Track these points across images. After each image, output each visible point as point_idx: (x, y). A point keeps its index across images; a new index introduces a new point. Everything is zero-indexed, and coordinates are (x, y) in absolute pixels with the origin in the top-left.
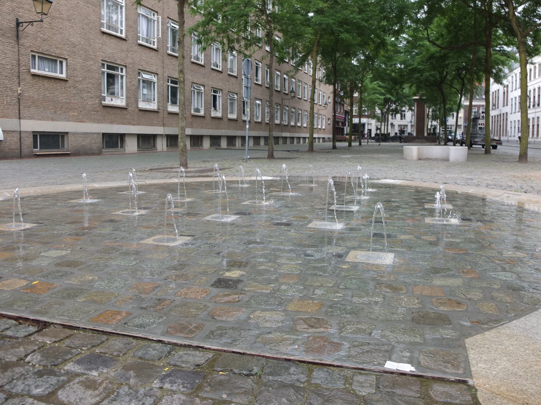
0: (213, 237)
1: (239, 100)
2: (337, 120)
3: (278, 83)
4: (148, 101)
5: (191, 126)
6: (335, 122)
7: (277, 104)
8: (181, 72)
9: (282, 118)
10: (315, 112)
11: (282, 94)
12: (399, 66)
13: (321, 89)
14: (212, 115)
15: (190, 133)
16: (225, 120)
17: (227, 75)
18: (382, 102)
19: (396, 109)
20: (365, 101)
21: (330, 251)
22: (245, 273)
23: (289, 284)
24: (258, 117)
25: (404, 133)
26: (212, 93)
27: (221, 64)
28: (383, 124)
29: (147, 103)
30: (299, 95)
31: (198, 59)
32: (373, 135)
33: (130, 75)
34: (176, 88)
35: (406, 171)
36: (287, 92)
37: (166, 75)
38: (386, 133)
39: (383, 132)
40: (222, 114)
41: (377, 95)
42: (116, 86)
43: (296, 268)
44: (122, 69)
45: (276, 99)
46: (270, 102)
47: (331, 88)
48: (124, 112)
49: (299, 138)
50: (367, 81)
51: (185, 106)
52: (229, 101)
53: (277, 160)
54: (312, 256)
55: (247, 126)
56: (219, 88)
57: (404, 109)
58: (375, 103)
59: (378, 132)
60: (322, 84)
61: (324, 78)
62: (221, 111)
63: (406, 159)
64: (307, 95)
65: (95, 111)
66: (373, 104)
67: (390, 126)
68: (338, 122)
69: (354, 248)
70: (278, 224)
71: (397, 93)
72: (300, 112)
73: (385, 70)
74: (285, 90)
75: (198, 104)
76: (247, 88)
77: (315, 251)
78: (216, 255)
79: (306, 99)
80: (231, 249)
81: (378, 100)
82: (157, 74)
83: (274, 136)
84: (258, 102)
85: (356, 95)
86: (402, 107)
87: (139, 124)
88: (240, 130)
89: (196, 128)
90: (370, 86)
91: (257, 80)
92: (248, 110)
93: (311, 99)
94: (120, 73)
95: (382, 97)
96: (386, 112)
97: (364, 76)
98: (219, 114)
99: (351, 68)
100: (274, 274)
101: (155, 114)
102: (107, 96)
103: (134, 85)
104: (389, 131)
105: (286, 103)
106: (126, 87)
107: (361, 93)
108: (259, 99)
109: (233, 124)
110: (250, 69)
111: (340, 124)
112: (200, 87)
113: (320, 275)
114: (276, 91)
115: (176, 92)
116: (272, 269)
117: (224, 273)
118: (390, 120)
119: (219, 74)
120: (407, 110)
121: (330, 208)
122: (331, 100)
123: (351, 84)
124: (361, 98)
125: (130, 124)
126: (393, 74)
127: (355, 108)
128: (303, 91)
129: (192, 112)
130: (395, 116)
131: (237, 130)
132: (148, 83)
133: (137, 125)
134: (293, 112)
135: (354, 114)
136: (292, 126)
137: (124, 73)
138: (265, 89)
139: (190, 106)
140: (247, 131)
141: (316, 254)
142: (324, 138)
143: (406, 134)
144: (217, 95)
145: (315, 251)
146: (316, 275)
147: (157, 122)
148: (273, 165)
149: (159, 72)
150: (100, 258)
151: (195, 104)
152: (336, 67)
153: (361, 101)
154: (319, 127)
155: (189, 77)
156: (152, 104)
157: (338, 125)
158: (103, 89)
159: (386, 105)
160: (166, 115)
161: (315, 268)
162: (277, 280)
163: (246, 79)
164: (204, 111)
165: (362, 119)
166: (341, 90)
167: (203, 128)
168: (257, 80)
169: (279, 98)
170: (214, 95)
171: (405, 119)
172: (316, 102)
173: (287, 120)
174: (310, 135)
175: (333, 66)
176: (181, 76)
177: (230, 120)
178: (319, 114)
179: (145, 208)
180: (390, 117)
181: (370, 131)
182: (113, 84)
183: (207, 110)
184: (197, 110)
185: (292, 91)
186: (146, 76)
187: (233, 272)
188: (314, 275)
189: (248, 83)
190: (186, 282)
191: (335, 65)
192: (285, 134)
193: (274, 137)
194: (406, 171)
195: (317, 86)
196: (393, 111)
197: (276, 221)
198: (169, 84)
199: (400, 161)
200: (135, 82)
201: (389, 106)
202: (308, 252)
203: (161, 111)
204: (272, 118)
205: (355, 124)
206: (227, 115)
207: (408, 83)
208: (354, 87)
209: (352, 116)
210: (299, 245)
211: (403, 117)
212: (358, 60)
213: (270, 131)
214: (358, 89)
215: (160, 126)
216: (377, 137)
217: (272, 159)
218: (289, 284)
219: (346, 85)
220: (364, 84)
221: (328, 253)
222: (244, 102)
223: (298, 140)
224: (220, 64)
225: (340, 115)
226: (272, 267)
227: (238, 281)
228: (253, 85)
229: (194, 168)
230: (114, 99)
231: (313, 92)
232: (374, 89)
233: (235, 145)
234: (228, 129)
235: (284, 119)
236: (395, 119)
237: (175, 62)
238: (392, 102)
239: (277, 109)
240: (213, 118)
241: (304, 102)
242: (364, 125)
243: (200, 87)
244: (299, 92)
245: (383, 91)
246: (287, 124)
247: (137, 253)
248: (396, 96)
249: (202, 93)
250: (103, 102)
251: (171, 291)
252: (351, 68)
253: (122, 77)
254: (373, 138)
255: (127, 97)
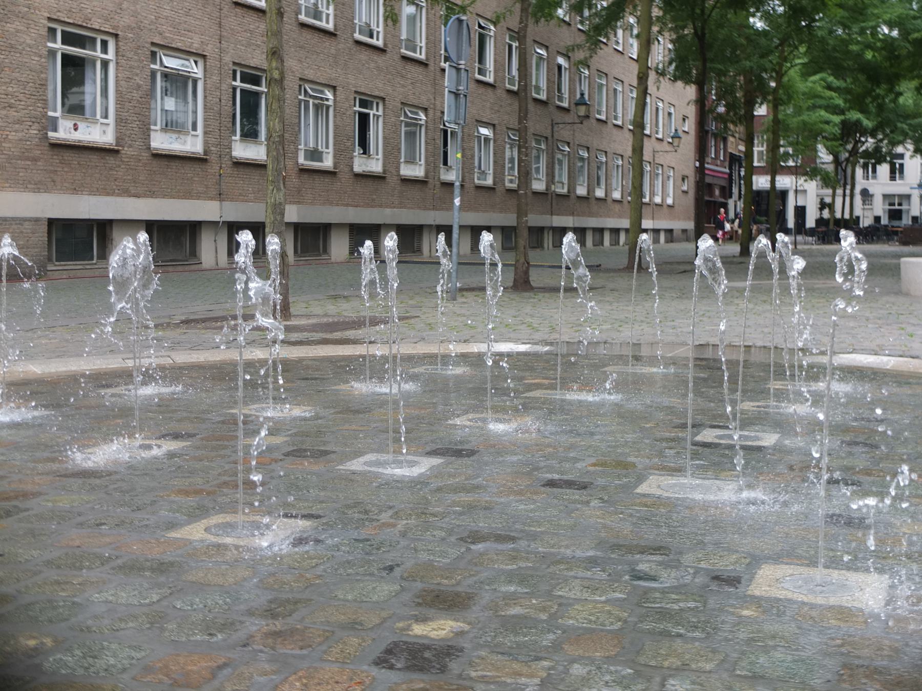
0: (372, 520)
1: (431, 126)
2: (708, 180)
3: (540, 80)
4: (172, 126)
5: (297, 197)
6: (703, 186)
7: (539, 138)
8: (274, 53)
9: (553, 177)
10: (644, 158)
11: (551, 108)
12: (886, 31)
13: (661, 94)
14: (357, 169)
15: (294, 219)
16: (392, 180)
17: (397, 58)
18: (837, 131)
19: (877, 149)
20: (787, 129)
21: (703, 565)
22: (466, 627)
23: (592, 661)
24: (483, 174)
25: (900, 218)
26: (357, 108)
27: (381, 29)
28: (839, 191)
29: (174, 136)
30: (599, 113)
31: (317, 15)
32: (810, 223)
33: (129, 59)
34: (257, 95)
35: (910, 329)
36: (565, 104)
37: (227, 59)
38: (847, 216)
39: (838, 215)
40: (384, 165)
41: (823, 113)
42: (88, 88)
43: (609, 612)
44: (104, 44)
45: (537, 123)
46: (522, 131)
47: (691, 91)
48: (111, 160)
49: (601, 231)
50: (793, 73)
51: (281, 144)
52: (403, 129)
53: (540, 295)
54: (653, 579)
55: (457, 201)
56: (376, 93)
57: (900, 149)
58: (817, 135)
59: (826, 214)
60: (665, 83)
61: (670, 63)
62: (380, 156)
63: (907, 294)
64: (625, 111)
65: (27, 159)
66: (809, 136)
67: (858, 199)
68: (710, 187)
69: (777, 559)
70: (551, 484)
71: (881, 108)
72: (604, 159)
73: (845, 43)
74: (560, 99)
75: (318, 141)
76: (456, 95)
77: (660, 563)
78: (384, 574)
79: (619, 123)
80: (424, 556)
81: (826, 127)
82: (204, 57)
83: (530, 224)
84: (484, 131)
85: (761, 111)
86: (894, 144)
87: (152, 194)
88: (434, 208)
89: (312, 204)
90: (802, 86)
91: (481, 72)
92: (455, 156)
93: (634, 123)
94: (99, 53)
95: (837, 119)
96: (847, 160)
97: (785, 59)
98: (375, 166)
99: (748, 38)
100: (549, 631)
101: (197, 167)
102: (63, 117)
103: (139, 86)
104: (858, 212)
105: (564, 133)
106: (117, 91)
107: (775, 106)
108: (486, 124)
109: (414, 193)
110: (465, 45)
111: (717, 192)
112: (322, 92)
113: (679, 635)
114: (536, 100)
115: (257, 106)
116: (544, 617)
117: (408, 628)
118: (861, 182)
119: (375, 56)
120: (908, 155)
121: (699, 438)
122: (690, 126)
123: (748, 82)
124: (776, 121)
125: (126, 193)
126: (869, 55)
127: (759, 148)
128: (612, 102)
129: (301, 160)
130: (874, 171)
131: (426, 209)
132: (178, 83)
133: (145, 196)
134: (582, 159)
135: (756, 164)
136: (580, 198)
137: (111, 55)
138: (504, 95)
139: (296, 142)
140: (456, 213)
141: (664, 574)
142: (670, 232)
143: (906, 221)
144: (372, 113)
145: (660, 563)
146: (666, 634)
147: (201, 189)
148: (528, 309)
149: (209, 50)
150: (58, 583)
151: (308, 137)
152: (704, 34)
153: (777, 128)
154: (658, 200)
155: (294, 65)
156: (189, 139)
157: (711, 194)
158: (50, 95)
159: (847, 142)
160: (227, 169)
161: (664, 615)
162: (557, 646)
163: (454, 71)
164: (335, 157)
165: (778, 178)
166: (719, 98)
167: (331, 204)
168: (481, 72)
169: (542, 120)
170: (361, 114)
171: (902, 178)
172: (647, 132)
173: (565, 181)
174: (632, 224)
175: (696, 33)
176: (274, 64)
177: (406, 181)
178: (655, 165)
179: (176, 436)
180: (859, 172)
181: (801, 212)
182: (81, 82)
183: (342, 153)
184: (315, 155)
185: (581, 102)
186: (172, 63)
187: (433, 625)
188: (661, 633)
189: (458, 83)
190: (305, 652)
191: (703, 28)
192: (558, 221)
193: (531, 229)
194: (910, 329)
195: (652, 88)
196: (867, 154)
197: (549, 476)
198: (238, 83)
199: (892, 299)
200: (141, 80)
201: (856, 142)
202: (642, 567)
203: (213, 158)
204: (525, 175)
205: (759, 193)
206: (398, 169)
207: (913, 78)
208: (756, 91)
209: (752, 171)
210: (616, 547)
211: (896, 172)
212: (767, 17)
213: (521, 213)
214: (768, 94)
215: (212, 199)
216: (823, 229)
217: (526, 290)
218: (592, 661)
219: (733, 85)
220: (785, 79)
221: (697, 571)
222: (445, 132)
223: (598, 236)
224: (379, 28)
225: (717, 167)
226: (544, 609)
227: (446, 652)
228: (472, 85)
229: (308, 316)
230: (81, 125)
231: (641, 106)
232: (813, 95)
233: (419, 251)
234: (401, 206)
235: (557, 179)
236: (874, 177)
237: (261, 25)
238: (864, 132)
239: (538, 150)
240: (358, 176)
241: (615, 131)
242: (784, 194)
243: (322, 92)
244: (600, 104)
245: (840, 102)
246: (565, 191)
247: (161, 568)
248: (878, 115)
249: (328, 107)
250: (51, 134)
251: (262, 679)
252: (748, 38)
253: (105, 64)
254: (811, 232)
255: (119, 121)
